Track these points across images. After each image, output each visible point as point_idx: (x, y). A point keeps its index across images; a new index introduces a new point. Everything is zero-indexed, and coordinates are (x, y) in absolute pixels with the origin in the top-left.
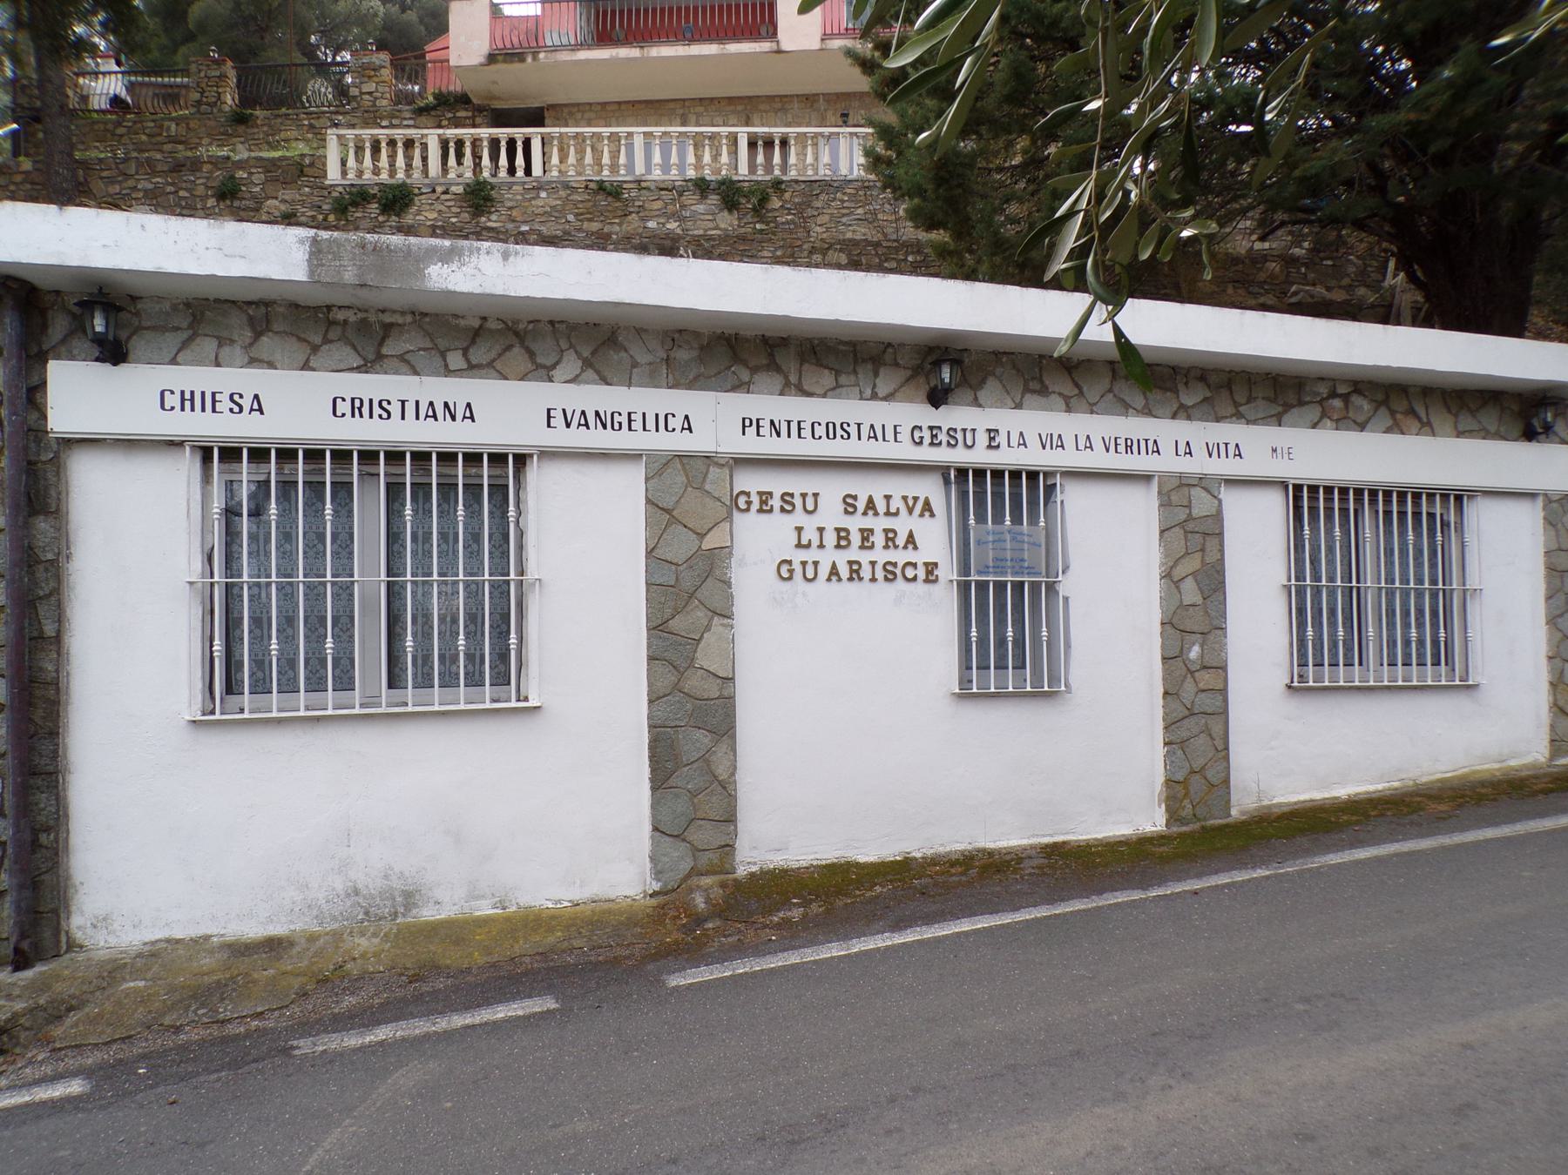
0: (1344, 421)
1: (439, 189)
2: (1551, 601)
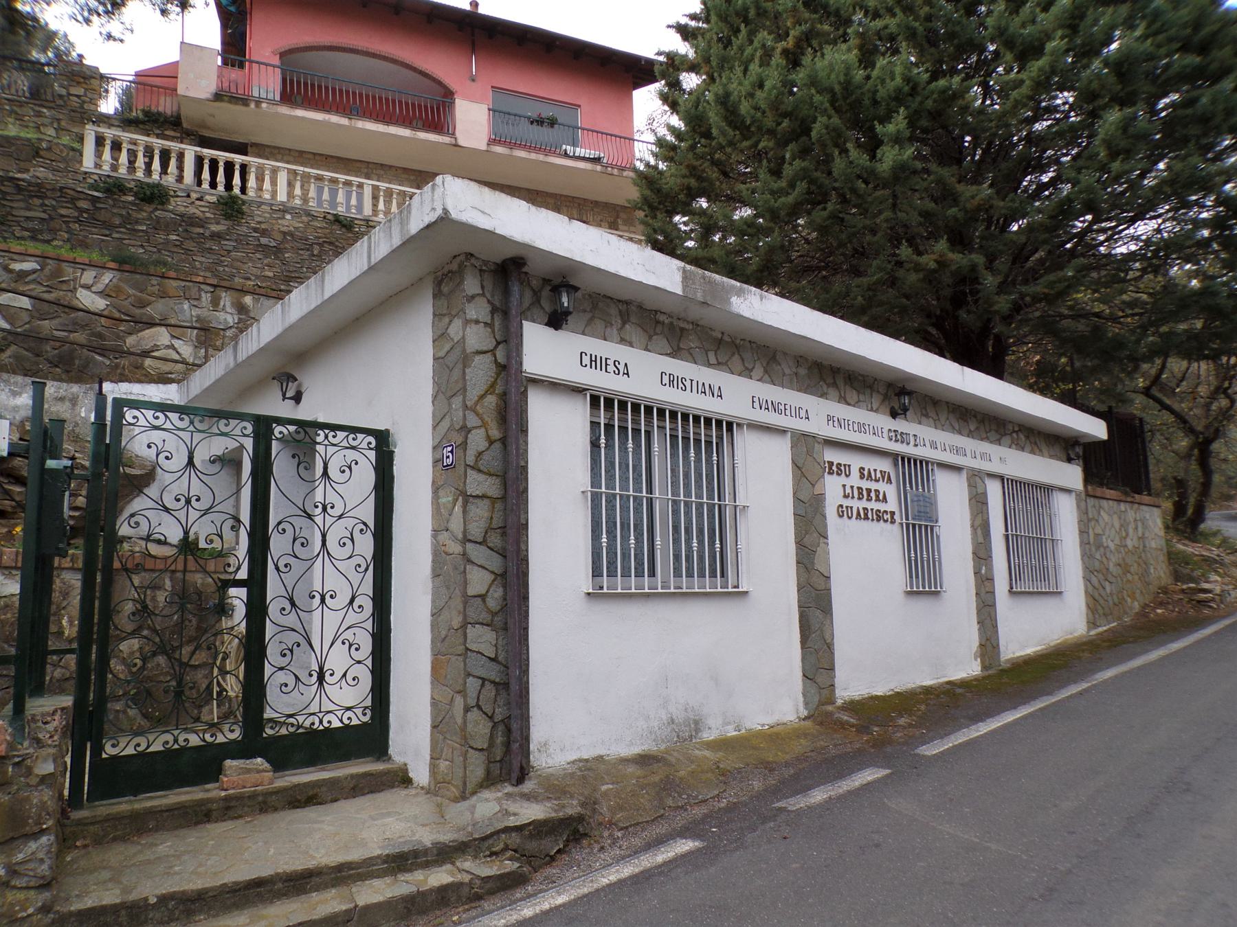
1: (194, 196)
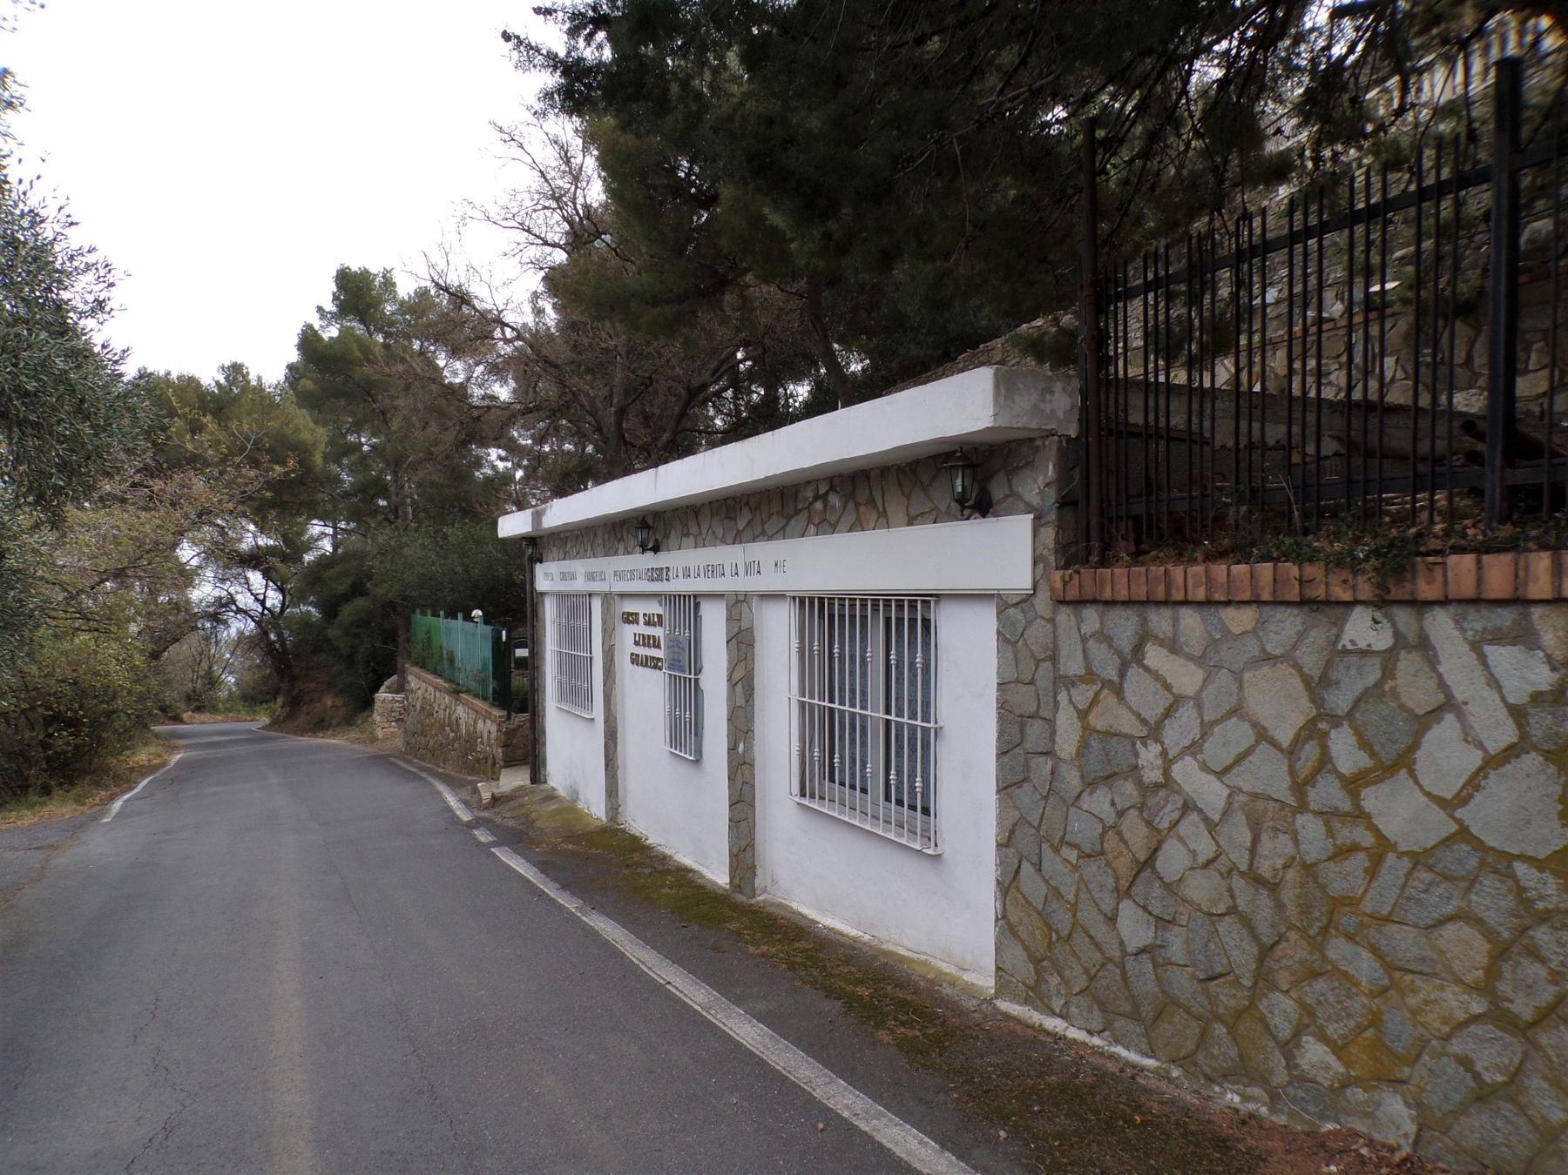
0: (827, 525)
2: (1006, 759)
